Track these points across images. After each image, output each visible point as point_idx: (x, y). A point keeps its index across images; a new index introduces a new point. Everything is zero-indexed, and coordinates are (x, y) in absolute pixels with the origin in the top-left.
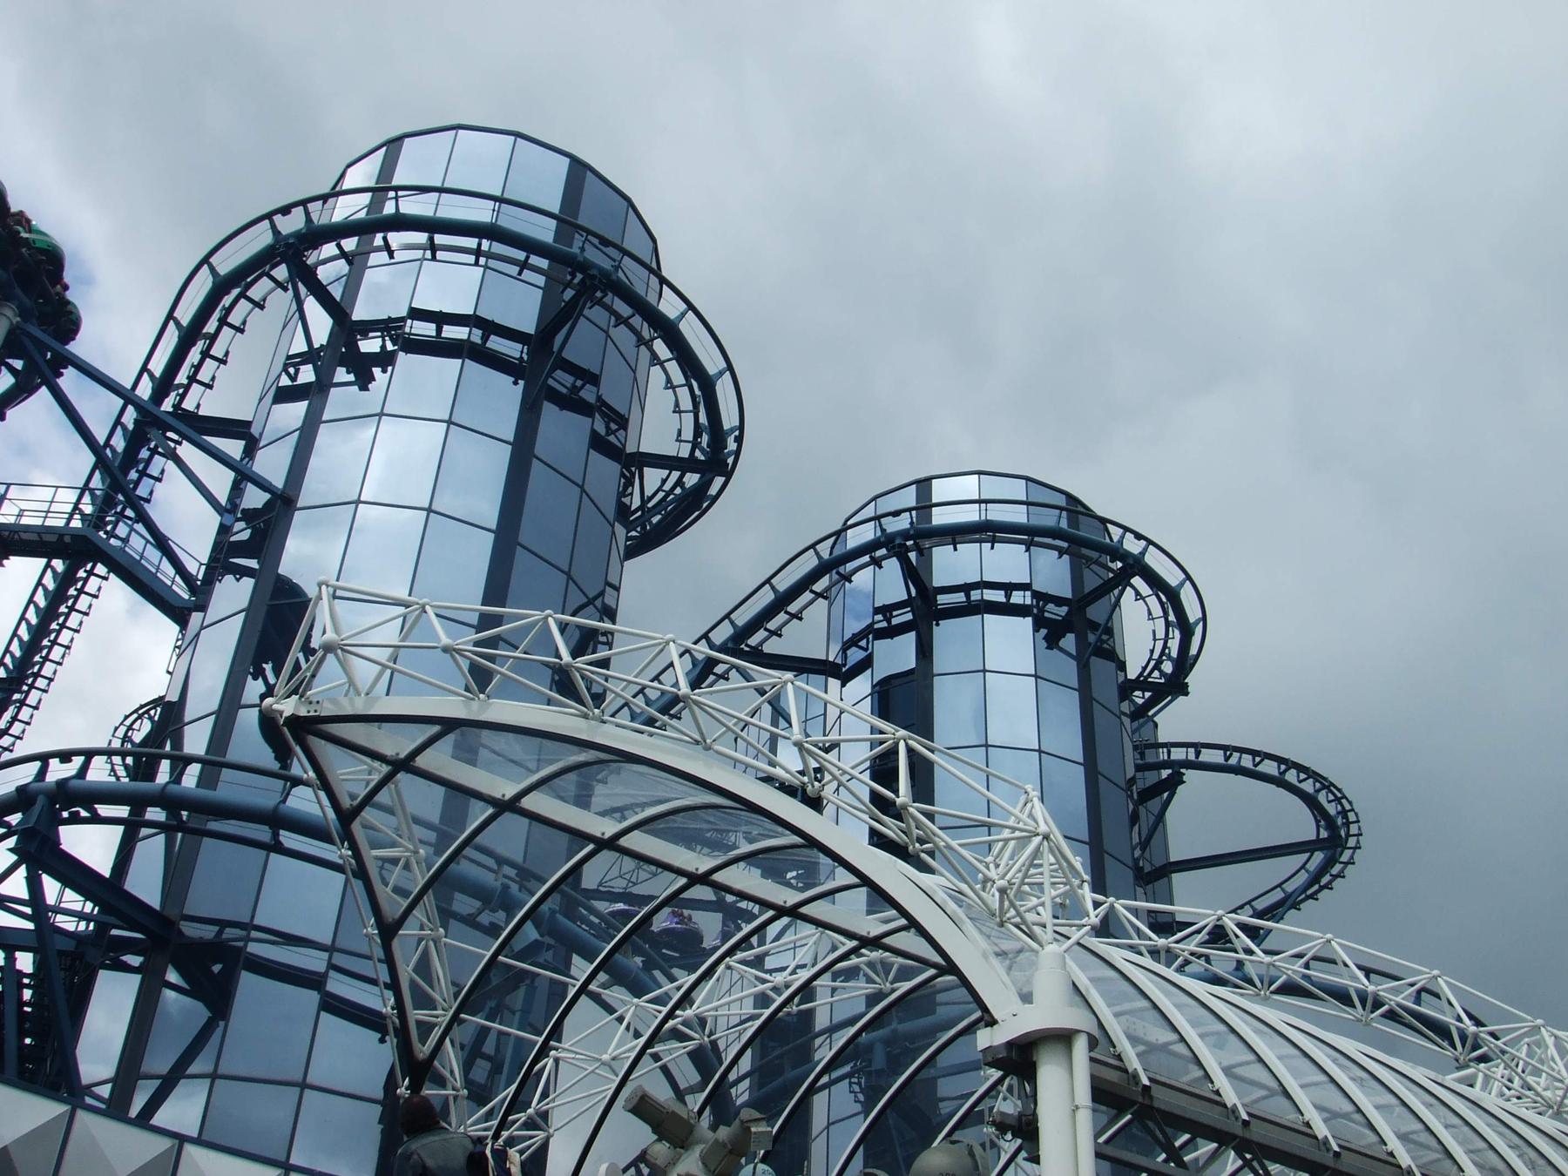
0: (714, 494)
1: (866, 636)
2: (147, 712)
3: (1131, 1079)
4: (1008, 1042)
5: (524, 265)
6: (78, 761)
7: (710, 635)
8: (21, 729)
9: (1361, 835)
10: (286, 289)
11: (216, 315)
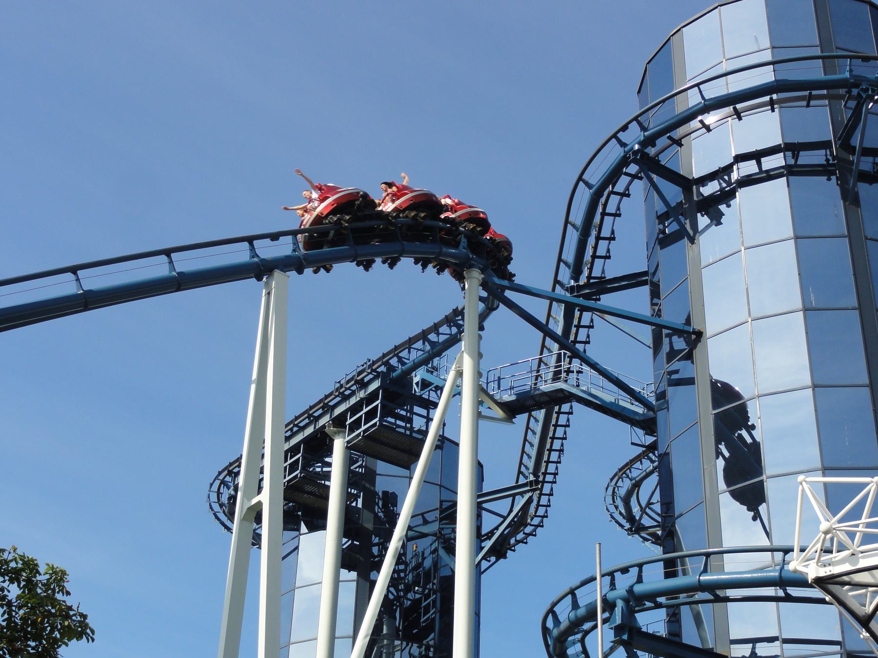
2: (624, 473)
5: (810, 98)
6: (634, 571)
8: (547, 500)
10: (641, 178)
11: (594, 233)
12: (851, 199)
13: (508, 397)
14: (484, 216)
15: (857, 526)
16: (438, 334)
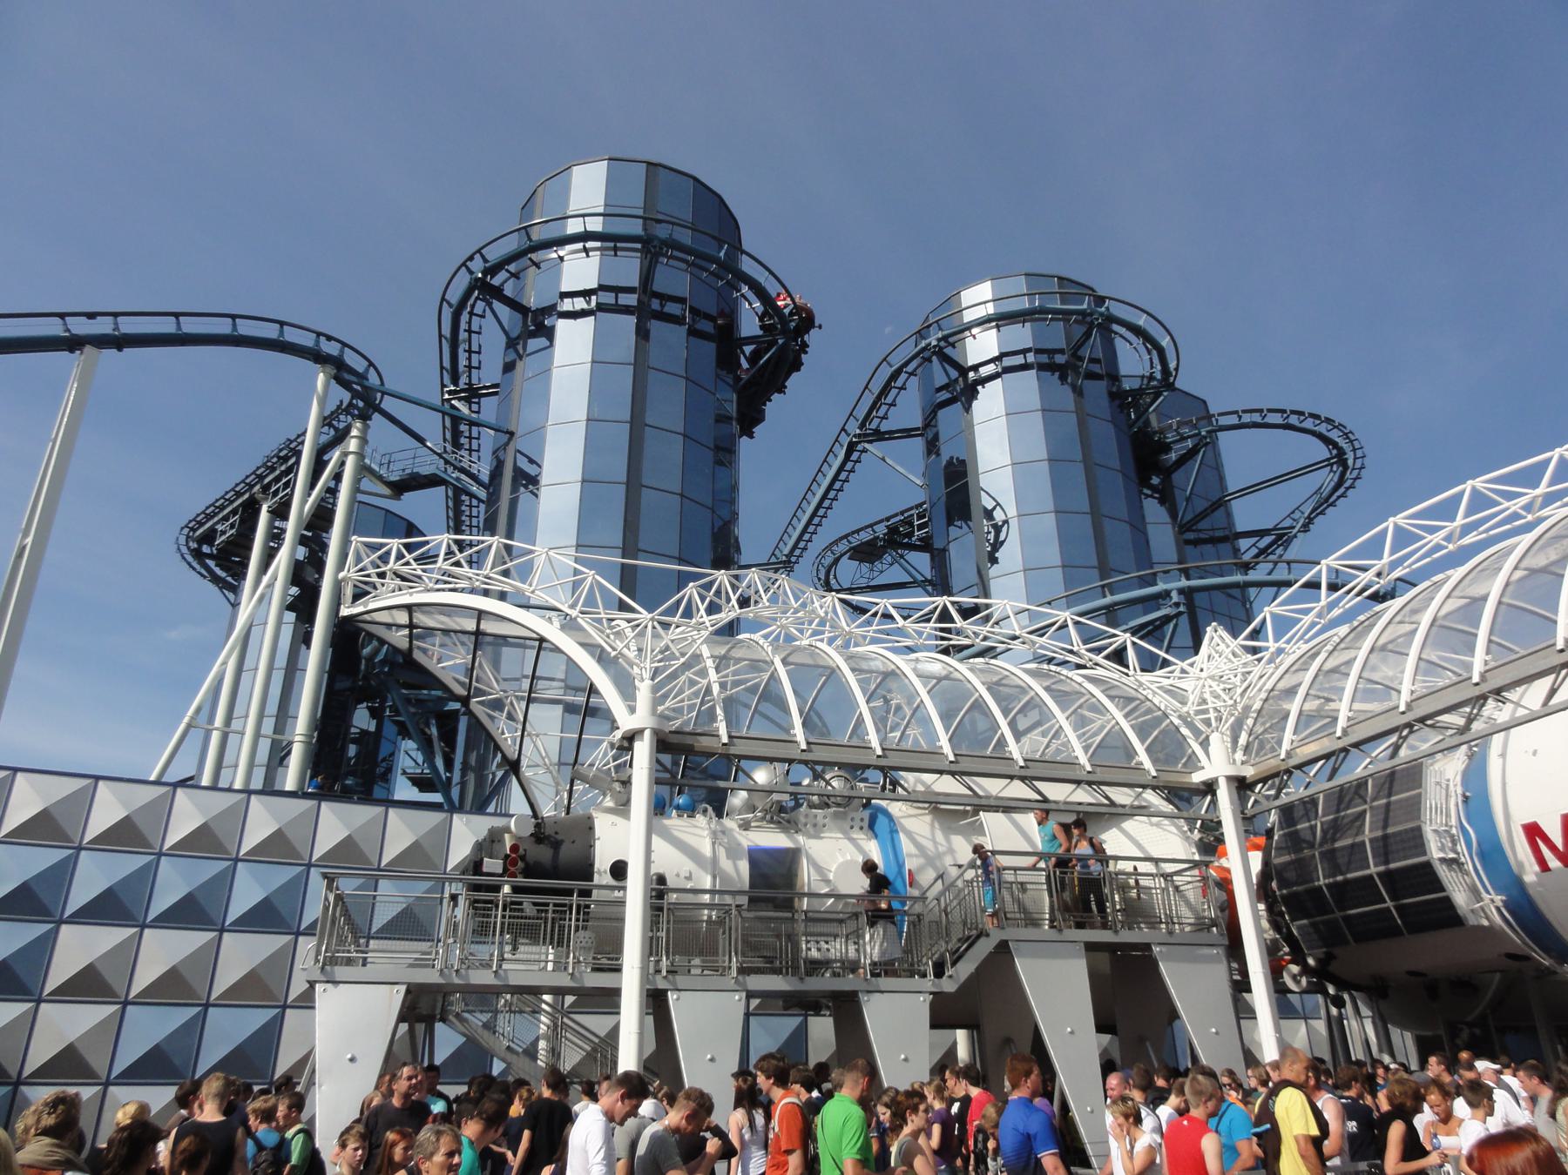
12: (642, 333)
13: (394, 478)
14: (720, 372)
15: (869, 631)
16: (339, 421)
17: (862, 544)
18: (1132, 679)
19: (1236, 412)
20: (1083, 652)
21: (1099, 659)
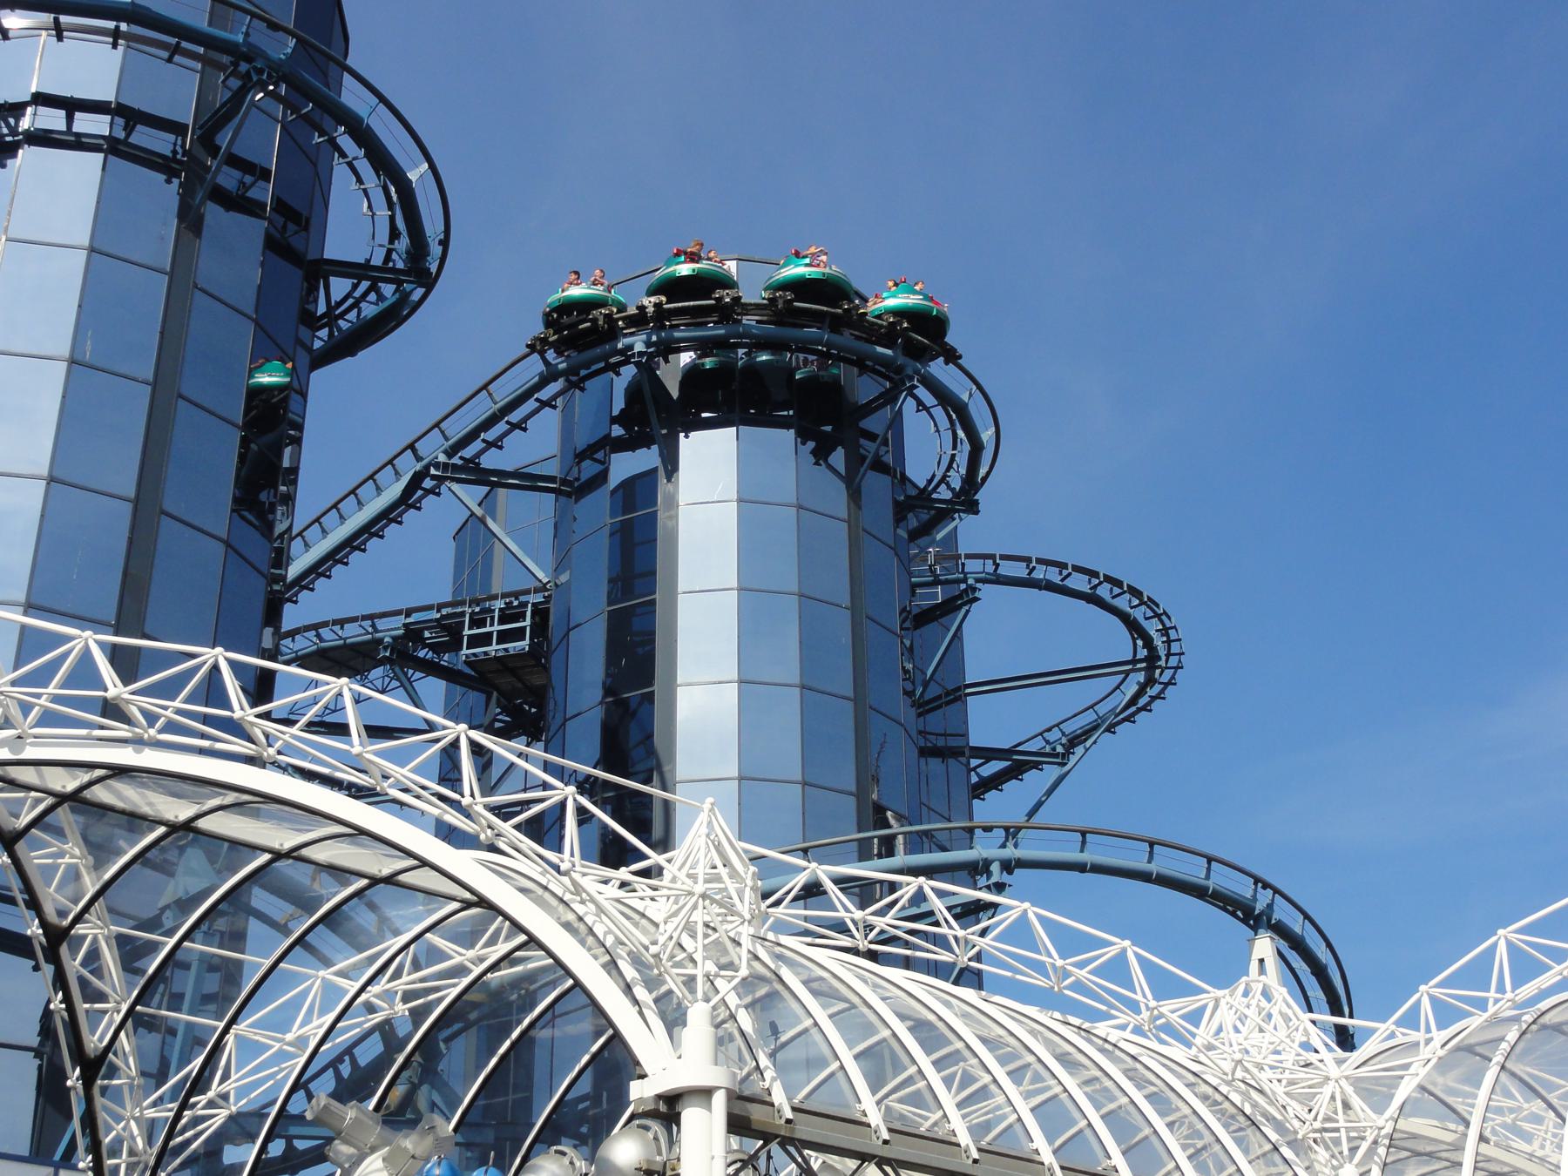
0: (417, 300)
1: (603, 447)
3: (776, 1112)
4: (656, 1095)
5: (176, 50)
7: (416, 445)
9: (1183, 654)
17: (345, 646)
18: (565, 880)
19: (1028, 560)
20: (479, 809)
21: (507, 827)
